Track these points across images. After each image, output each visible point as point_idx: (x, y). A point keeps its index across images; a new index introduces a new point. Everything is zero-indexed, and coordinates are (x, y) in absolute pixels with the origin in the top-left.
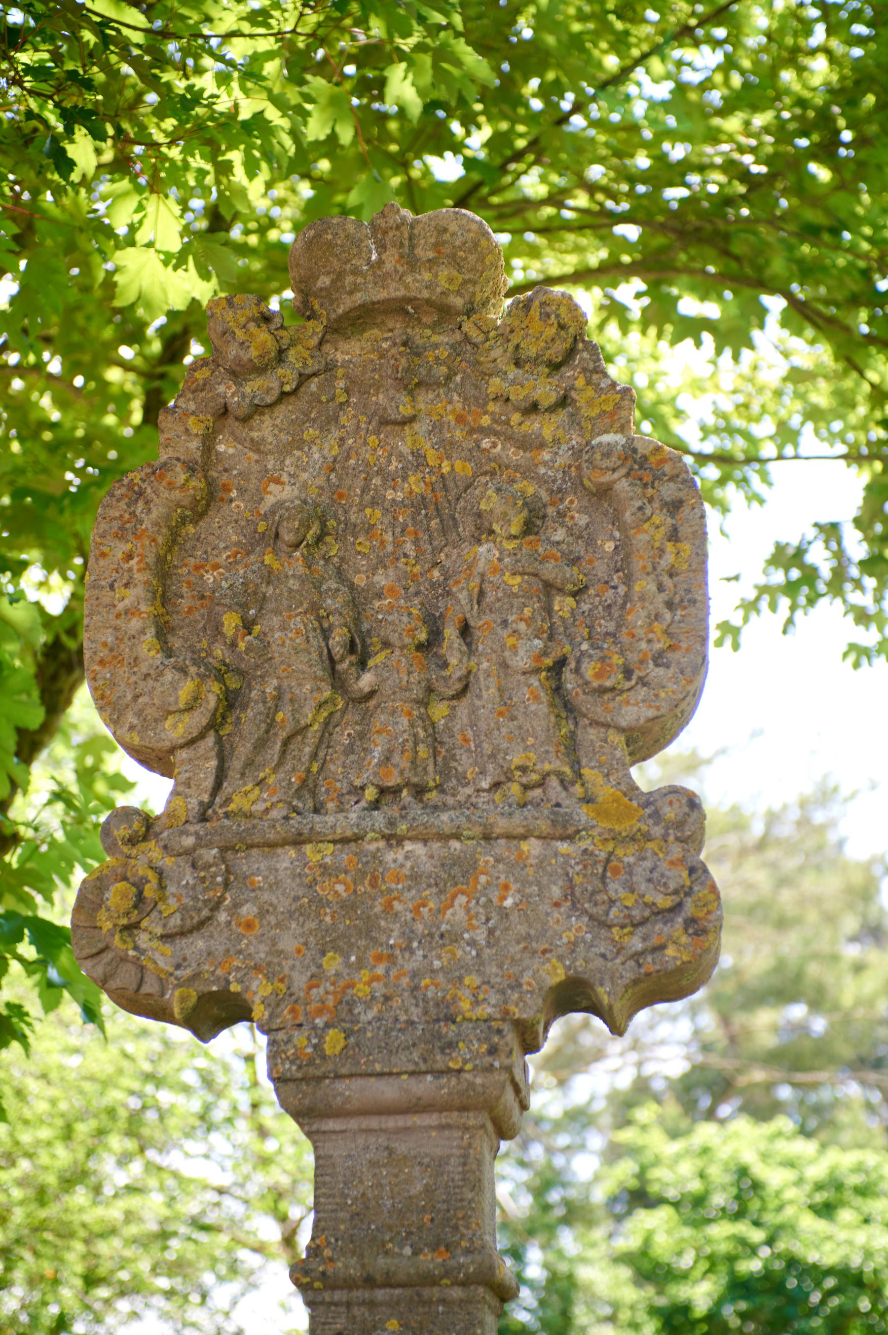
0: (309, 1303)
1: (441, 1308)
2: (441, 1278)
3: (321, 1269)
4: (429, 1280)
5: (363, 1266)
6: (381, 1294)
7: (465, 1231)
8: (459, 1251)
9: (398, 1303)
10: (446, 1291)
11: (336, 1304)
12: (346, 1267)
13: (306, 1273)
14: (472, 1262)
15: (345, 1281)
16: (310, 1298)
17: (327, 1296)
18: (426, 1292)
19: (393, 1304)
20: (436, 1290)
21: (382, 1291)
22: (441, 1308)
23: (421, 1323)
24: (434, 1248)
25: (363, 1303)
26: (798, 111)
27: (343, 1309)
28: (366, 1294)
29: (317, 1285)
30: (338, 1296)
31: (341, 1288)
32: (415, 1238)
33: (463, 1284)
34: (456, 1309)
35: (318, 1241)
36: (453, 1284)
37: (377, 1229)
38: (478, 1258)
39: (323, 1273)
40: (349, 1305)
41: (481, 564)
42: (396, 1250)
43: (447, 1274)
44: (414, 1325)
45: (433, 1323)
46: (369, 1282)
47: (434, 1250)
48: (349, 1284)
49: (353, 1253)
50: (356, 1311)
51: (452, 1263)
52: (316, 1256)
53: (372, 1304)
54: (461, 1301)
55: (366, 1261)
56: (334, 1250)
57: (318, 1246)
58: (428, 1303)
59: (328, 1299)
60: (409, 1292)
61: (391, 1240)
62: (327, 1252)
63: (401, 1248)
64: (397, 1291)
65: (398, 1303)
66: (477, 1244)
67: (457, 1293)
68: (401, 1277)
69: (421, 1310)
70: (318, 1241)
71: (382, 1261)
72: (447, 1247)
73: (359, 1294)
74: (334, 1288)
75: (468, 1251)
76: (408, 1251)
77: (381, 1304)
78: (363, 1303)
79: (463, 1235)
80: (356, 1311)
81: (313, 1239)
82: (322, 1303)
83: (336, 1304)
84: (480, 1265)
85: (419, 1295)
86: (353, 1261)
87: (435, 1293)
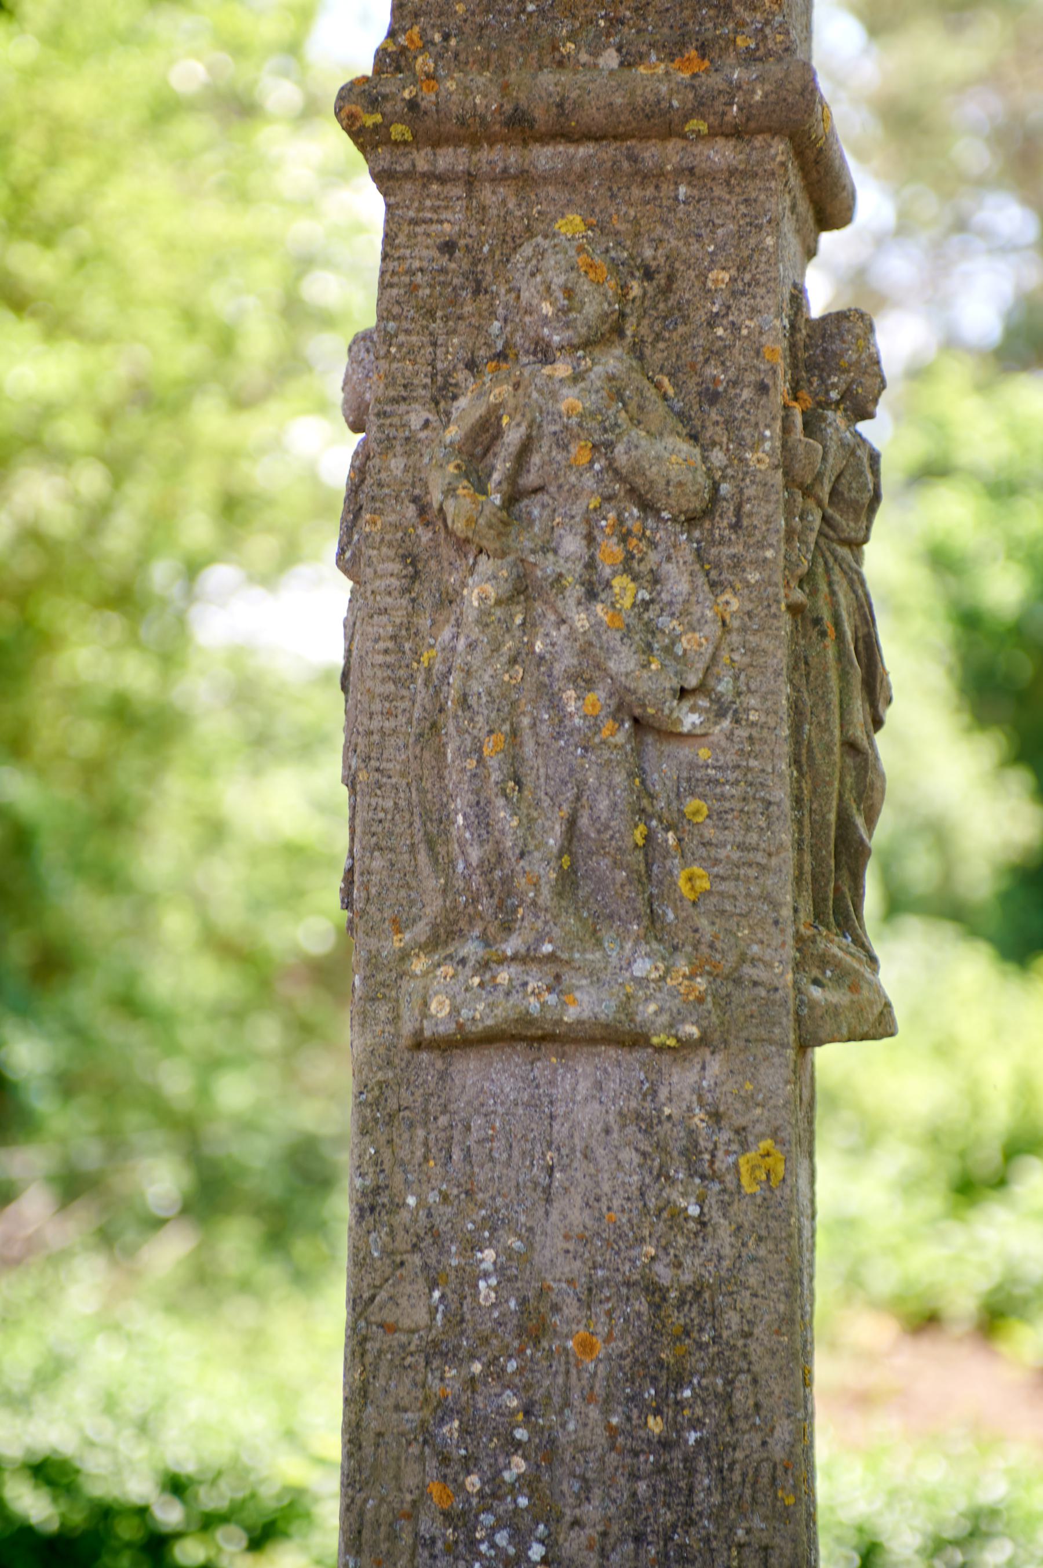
0: (383, 178)
1: (683, 190)
2: (686, 118)
3: (406, 95)
4: (659, 123)
5: (505, 88)
6: (545, 157)
7: (747, 16)
8: (731, 59)
9: (583, 177)
10: (699, 148)
11: (442, 179)
12: (466, 91)
13: (374, 102)
14: (761, 79)
15: (462, 122)
16: (384, 164)
17: (422, 159)
18: (650, 152)
19: (571, 180)
20: (673, 145)
21: (548, 150)
22: (683, 190)
23: (636, 222)
24: (673, 51)
25: (504, 176)
26: (632, 1300)
27: (458, 190)
28: (512, 157)
29: (399, 131)
30: (448, 159)
31: (455, 141)
32: (628, 32)
33: (737, 133)
34: (719, 191)
35: (402, 40)
36: (714, 133)
37: (541, 11)
38: (775, 69)
39: (413, 105)
40: (470, 180)
41: (739, 1455)
42: (584, 57)
43: (699, 107)
44: (621, 227)
45: (666, 223)
46: (520, 127)
47: (671, 57)
48: (472, 133)
49: (484, 64)
50: (487, 195)
51: (716, 81)
52: (399, 69)
53: (524, 179)
54: (732, 172)
55: (513, 77)
56: (440, 56)
57: (403, 50)
58: (653, 177)
59: (422, 166)
60: (609, 151)
61: (572, 37)
62: (424, 63)
63: (595, 54)
64: (583, 151)
65: (583, 177)
66: (775, 41)
67: (722, 154)
68: (593, 114)
69: (636, 192)
70: (402, 40)
71: (548, 79)
72: (703, 50)
73: (493, 156)
74: (437, 142)
75: (750, 57)
76: (610, 59)
77: (545, 179)
78: (504, 176)
79: (741, 24)
80: (487, 195)
81: (392, 34)
82: (409, 175)
83: (442, 179)
84: (780, 85)
85: (633, 158)
86: (483, 79)
87: (671, 153)
